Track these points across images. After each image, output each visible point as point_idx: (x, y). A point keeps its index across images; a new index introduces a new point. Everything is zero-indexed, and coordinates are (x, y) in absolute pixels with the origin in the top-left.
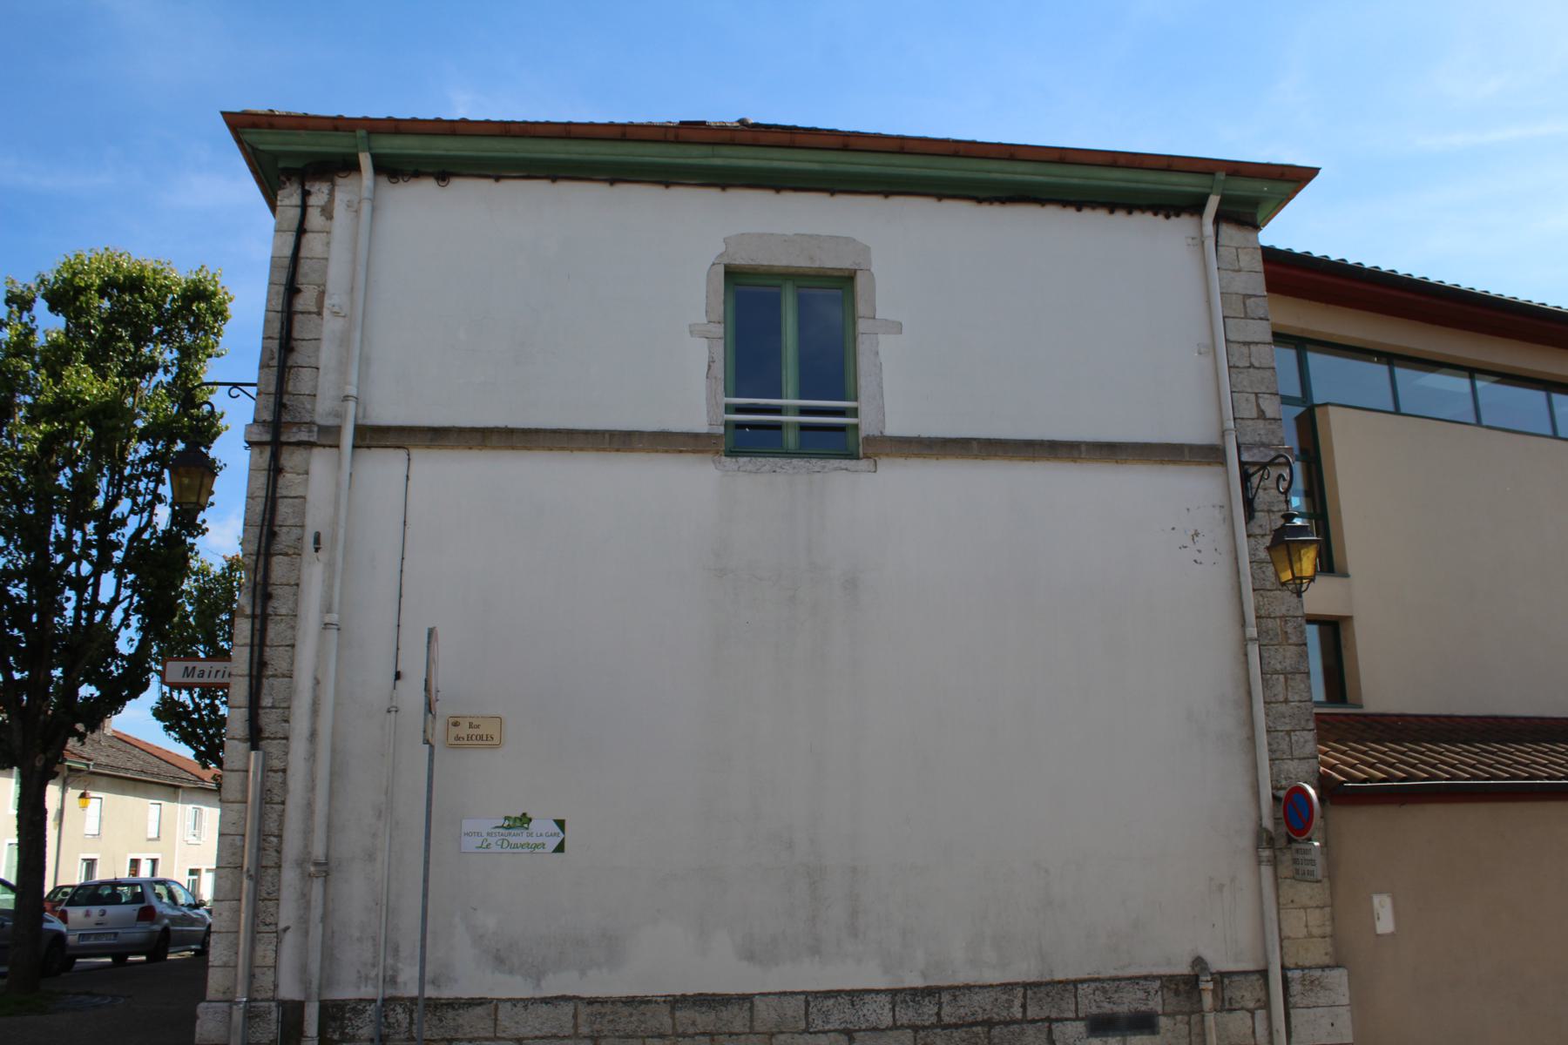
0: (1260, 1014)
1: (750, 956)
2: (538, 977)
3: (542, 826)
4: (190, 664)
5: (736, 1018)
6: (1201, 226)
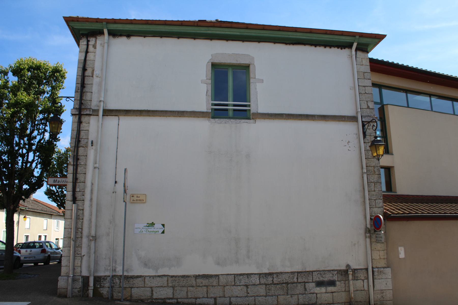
0: (366, 281)
1: (218, 264)
2: (157, 269)
3: (158, 226)
4: (55, 179)
5: (214, 281)
6: (351, 52)
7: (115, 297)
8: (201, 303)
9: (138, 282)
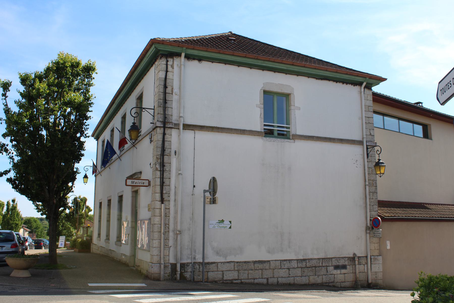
1: (269, 252)
2: (226, 257)
4: (133, 180)
5: (266, 266)
6: (361, 89)
7: (196, 280)
9: (212, 267)
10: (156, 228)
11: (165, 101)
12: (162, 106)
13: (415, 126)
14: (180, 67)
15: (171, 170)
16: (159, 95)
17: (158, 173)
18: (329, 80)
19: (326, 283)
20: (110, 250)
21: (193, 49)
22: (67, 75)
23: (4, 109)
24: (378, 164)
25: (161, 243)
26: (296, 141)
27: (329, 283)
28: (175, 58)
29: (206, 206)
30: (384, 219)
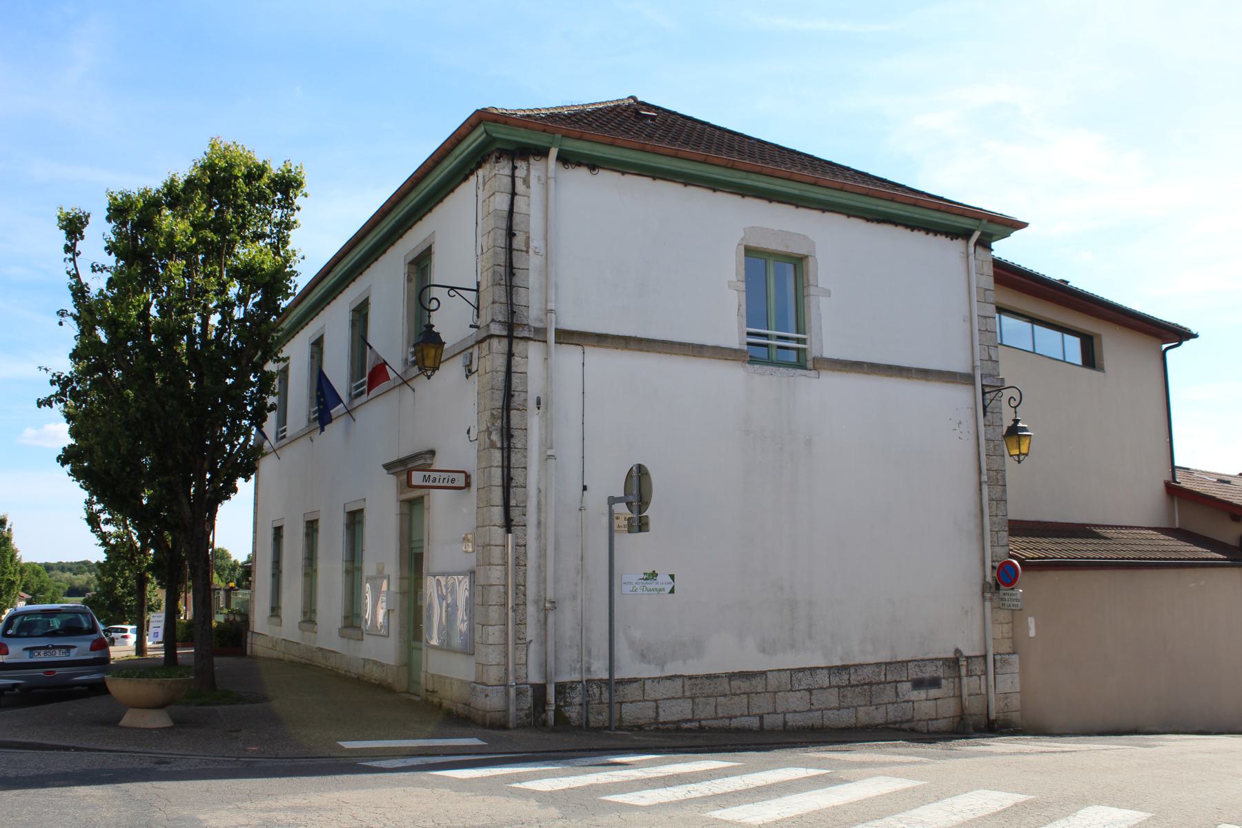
0: (983, 677)
1: (763, 651)
2: (662, 665)
3: (663, 578)
4: (427, 474)
5: (758, 684)
6: (967, 246)
7: (592, 724)
8: (739, 726)
9: (632, 691)
10: (494, 596)
11: (511, 270)
12: (503, 282)
13: (1067, 337)
14: (546, 185)
15: (529, 447)
16: (495, 254)
17: (497, 456)
18: (896, 224)
19: (895, 723)
20: (321, 649)
21: (580, 139)
22: (236, 194)
23: (71, 287)
24: (1014, 432)
25: (507, 634)
26: (823, 373)
27: (902, 722)
28: (532, 161)
29: (617, 538)
30: (1026, 566)
